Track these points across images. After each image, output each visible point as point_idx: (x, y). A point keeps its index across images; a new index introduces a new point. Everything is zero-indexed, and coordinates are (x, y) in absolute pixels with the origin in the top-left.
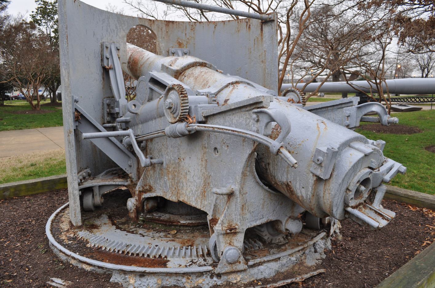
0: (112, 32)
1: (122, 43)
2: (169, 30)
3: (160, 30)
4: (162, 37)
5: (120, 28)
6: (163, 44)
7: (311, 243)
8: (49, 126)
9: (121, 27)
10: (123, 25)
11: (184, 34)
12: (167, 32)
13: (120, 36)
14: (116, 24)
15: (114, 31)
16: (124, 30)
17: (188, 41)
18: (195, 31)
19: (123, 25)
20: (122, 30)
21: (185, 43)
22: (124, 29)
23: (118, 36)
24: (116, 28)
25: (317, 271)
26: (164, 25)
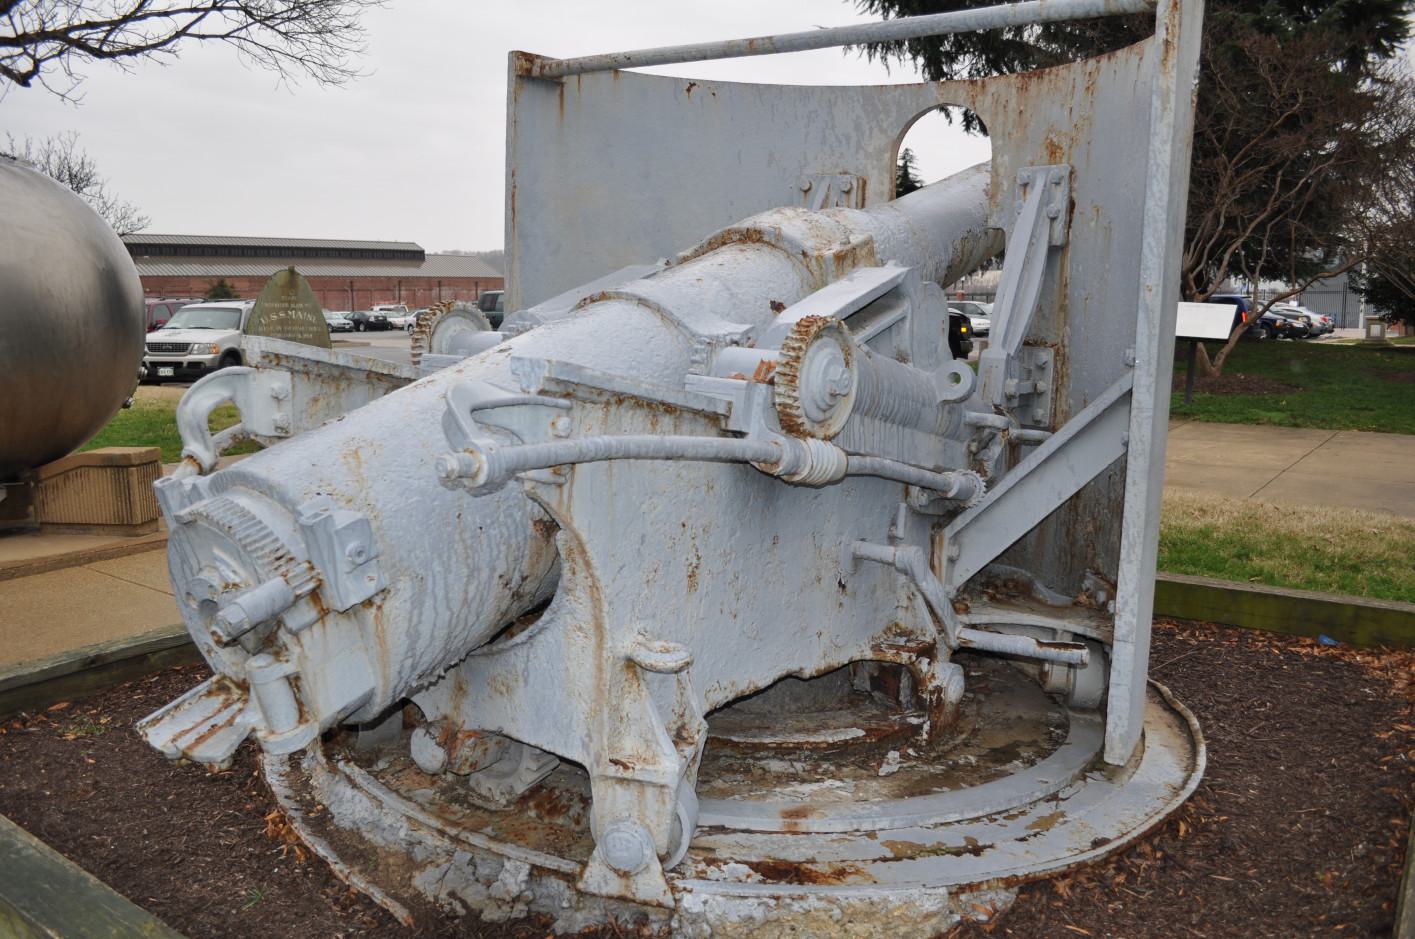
0: (840, 142)
1: (876, 171)
2: (1026, 105)
3: (1000, 109)
4: (1003, 134)
5: (871, 129)
6: (1006, 158)
7: (354, 800)
8: (1393, 430)
9: (874, 124)
10: (882, 116)
11: (1066, 112)
12: (1021, 112)
13: (870, 149)
14: (858, 117)
15: (848, 138)
16: (883, 131)
17: (1074, 134)
18: (1095, 94)
19: (882, 116)
20: (876, 131)
21: (1065, 145)
22: (885, 126)
23: (861, 152)
24: (858, 127)
25: (388, 901)
26: (1014, 91)
